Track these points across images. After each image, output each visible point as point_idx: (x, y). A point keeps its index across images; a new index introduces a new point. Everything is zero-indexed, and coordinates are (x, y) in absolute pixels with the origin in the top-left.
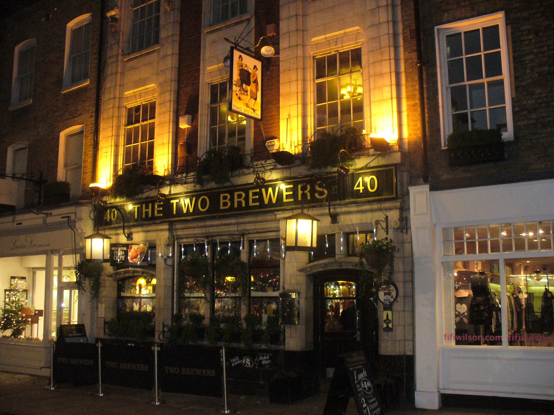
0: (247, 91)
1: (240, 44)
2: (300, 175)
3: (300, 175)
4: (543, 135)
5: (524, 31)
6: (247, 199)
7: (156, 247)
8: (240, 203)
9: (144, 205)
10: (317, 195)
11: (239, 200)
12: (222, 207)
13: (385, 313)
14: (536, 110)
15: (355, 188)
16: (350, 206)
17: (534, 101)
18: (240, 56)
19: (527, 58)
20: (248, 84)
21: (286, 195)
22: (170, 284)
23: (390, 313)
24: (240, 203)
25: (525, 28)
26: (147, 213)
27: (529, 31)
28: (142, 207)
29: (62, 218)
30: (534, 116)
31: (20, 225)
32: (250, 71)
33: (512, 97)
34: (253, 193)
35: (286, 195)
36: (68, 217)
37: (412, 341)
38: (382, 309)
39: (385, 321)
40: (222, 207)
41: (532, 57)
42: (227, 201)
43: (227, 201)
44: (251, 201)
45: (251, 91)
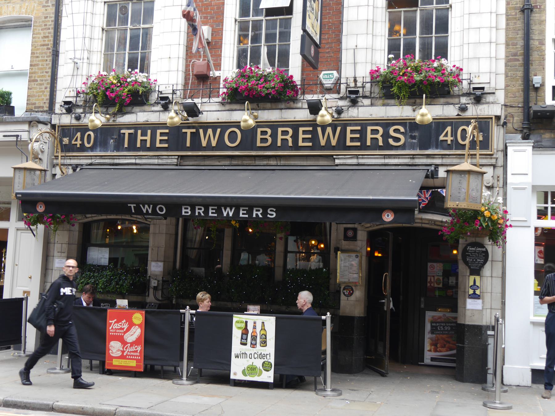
2: (370, 116)
3: (370, 116)
6: (295, 137)
7: (11, 204)
8: (284, 141)
12: (259, 144)
13: (472, 278)
16: (434, 157)
22: (173, 232)
23: (478, 278)
24: (284, 141)
28: (136, 133)
29: (4, 136)
33: (535, 263)
36: (17, 136)
38: (468, 274)
39: (471, 286)
40: (259, 144)
43: (267, 137)
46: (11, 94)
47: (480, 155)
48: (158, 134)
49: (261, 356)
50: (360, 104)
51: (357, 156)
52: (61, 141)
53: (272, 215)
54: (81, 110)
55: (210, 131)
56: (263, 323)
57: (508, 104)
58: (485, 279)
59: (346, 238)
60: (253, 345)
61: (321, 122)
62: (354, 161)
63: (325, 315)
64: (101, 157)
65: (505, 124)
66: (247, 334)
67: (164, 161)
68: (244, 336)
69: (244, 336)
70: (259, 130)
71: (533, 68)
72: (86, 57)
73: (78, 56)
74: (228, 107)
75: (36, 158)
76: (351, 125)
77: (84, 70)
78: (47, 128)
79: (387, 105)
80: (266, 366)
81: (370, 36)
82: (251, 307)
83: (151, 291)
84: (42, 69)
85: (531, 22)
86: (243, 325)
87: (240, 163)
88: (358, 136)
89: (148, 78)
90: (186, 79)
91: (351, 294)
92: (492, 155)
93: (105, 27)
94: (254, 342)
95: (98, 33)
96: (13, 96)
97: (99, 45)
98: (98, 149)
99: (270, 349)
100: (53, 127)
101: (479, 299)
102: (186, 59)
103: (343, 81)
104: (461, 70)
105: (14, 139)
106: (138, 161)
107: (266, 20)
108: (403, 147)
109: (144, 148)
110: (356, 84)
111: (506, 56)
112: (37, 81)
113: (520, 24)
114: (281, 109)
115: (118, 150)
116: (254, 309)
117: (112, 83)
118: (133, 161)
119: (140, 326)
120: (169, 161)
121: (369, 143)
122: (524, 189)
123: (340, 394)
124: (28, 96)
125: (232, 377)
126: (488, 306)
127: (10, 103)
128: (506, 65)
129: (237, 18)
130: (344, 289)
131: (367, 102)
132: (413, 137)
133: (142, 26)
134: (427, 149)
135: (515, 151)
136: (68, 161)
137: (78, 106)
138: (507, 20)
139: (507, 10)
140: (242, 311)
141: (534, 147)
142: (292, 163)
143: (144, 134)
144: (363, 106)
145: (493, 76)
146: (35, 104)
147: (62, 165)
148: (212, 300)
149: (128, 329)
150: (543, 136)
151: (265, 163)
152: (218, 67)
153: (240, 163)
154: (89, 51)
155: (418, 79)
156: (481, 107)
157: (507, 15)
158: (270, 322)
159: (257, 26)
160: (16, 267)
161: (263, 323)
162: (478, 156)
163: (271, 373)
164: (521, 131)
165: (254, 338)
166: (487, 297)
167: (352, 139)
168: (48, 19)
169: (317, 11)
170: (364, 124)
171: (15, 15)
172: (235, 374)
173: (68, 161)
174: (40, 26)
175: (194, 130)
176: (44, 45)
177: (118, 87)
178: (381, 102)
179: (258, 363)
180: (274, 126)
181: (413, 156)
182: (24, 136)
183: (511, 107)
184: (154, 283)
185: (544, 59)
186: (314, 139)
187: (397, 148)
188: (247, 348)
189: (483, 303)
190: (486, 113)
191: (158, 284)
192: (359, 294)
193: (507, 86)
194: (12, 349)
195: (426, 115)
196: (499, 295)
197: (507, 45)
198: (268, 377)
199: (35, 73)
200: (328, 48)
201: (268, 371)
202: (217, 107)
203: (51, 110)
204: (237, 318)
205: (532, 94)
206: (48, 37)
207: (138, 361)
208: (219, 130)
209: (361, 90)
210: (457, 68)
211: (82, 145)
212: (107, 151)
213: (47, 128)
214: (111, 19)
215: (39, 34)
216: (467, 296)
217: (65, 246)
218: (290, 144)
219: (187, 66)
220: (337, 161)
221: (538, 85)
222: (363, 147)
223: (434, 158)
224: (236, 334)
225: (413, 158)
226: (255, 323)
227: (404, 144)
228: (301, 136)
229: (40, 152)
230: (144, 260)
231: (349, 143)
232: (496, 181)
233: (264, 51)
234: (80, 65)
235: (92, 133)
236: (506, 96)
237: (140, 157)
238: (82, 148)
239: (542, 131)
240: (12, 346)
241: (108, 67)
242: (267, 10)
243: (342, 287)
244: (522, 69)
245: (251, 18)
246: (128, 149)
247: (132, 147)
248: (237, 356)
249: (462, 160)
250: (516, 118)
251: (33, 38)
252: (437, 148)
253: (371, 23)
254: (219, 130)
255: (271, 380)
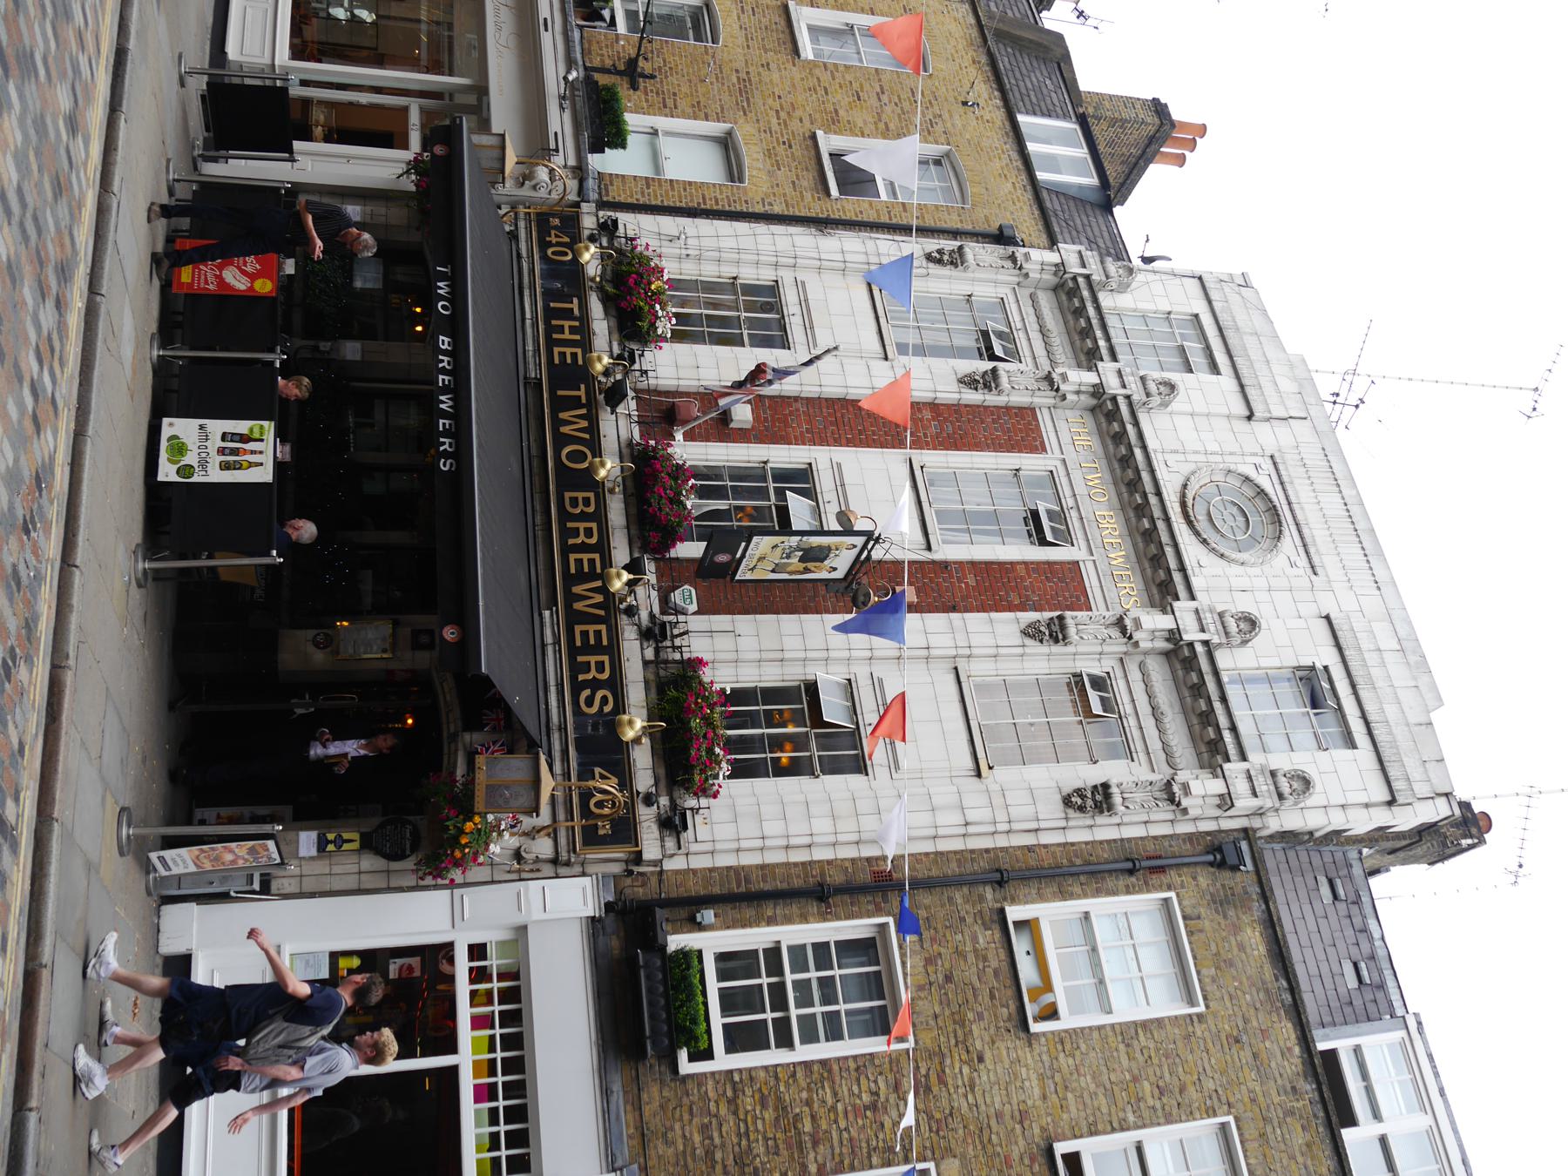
0: (788, 557)
1: (877, 546)
4: (687, 1128)
5: (876, 1082)
6: (584, 548)
8: (576, 532)
9: (577, 324)
10: (587, 692)
11: (580, 501)
12: (568, 495)
13: (356, 836)
14: (735, 1113)
15: (597, 770)
17: (749, 1108)
18: (855, 546)
19: (828, 1090)
20: (802, 560)
21: (565, 353)
23: (356, 845)
24: (576, 532)
25: (882, 1084)
26: (561, 329)
27: (877, 1094)
29: (545, 19)
30: (723, 1111)
31: (542, 28)
32: (826, 562)
34: (600, 632)
35: (565, 353)
36: (557, 150)
37: (298, 891)
38: (363, 830)
40: (568, 495)
41: (830, 1100)
42: (581, 507)
43: (581, 507)
44: (579, 556)
45: (790, 564)
46: (624, 147)
47: (573, 828)
48: (574, 350)
49: (203, 464)
50: (645, 645)
51: (557, 642)
52: (554, 216)
53: (445, 465)
54: (605, 243)
55: (584, 424)
56: (261, 464)
57: (665, 877)
58: (354, 858)
59: (416, 633)
60: (221, 451)
61: (608, 574)
62: (549, 639)
63: (279, 555)
64: (532, 271)
65: (630, 873)
66: (240, 442)
67: (531, 360)
68: (238, 438)
69: (238, 438)
70: (591, 495)
71: (730, 912)
72: (689, 252)
73: (690, 241)
74: (625, 451)
75: (525, 178)
76: (609, 630)
77: (667, 250)
78: (573, 197)
79: (647, 689)
80: (186, 470)
81: (757, 656)
82: (288, 448)
83: (312, 343)
84: (667, 195)
85: (803, 901)
86: (256, 435)
87: (535, 470)
88: (592, 642)
89: (664, 339)
90: (667, 393)
91: (317, 645)
92: (575, 851)
93: (739, 281)
94: (227, 451)
95: (728, 271)
96: (621, 151)
97: (709, 272)
98: (544, 267)
99: (216, 476)
100: (577, 205)
101: (319, 851)
102: (699, 393)
103: (681, 618)
104: (715, 796)
105: (552, 146)
106: (528, 322)
107: (770, 507)
108: (577, 711)
109: (550, 330)
110: (677, 636)
111: (743, 867)
112: (648, 188)
113: (797, 883)
114: (628, 527)
115: (543, 294)
116: (285, 453)
117: (650, 283)
118: (528, 315)
119: (251, 288)
120: (531, 366)
121: (580, 659)
122: (520, 909)
123: (139, 586)
124: (623, 176)
125: (166, 421)
126: (307, 869)
127: (610, 147)
128: (729, 868)
129: (770, 465)
130: (326, 635)
131: (650, 654)
132: (595, 727)
133: (745, 332)
134: (578, 749)
135: (584, 889)
136: (522, 224)
137: (611, 241)
138: (803, 864)
139: (819, 862)
140: (281, 434)
141: (593, 918)
142: (540, 548)
143: (573, 330)
144: (642, 649)
145: (708, 847)
146: (612, 184)
147: (516, 214)
148: (298, 400)
149: (244, 273)
150: (614, 937)
151: (538, 507)
152: (689, 437)
153: (535, 470)
154: (699, 258)
155: (693, 724)
156: (655, 827)
157: (811, 863)
158: (264, 475)
159: (762, 493)
160: (345, 160)
161: (261, 464)
162: (570, 824)
163: (174, 478)
164: (618, 899)
165: (235, 452)
166: (321, 867)
167: (585, 634)
168: (744, 205)
169: (789, 569)
170: (614, 650)
171: (747, 162)
172: (171, 425)
173: (522, 224)
174: (733, 194)
175: (584, 401)
176: (704, 198)
177: (646, 293)
178: (651, 677)
179: (191, 458)
180: (600, 516)
181: (563, 728)
182: (558, 161)
183: (660, 881)
184: (325, 346)
185: (744, 926)
186: (582, 577)
187: (576, 702)
188: (216, 442)
189: (312, 858)
190: (645, 836)
191: (324, 352)
192: (319, 657)
193: (694, 872)
194: (206, 134)
195: (632, 728)
196: (327, 888)
197: (763, 867)
198: (167, 472)
199: (660, 185)
200: (733, 597)
201: (178, 472)
202: (624, 434)
203: (602, 205)
204: (269, 427)
205: (683, 913)
206: (717, 203)
207: (191, 285)
208: (587, 436)
209: (668, 643)
210: (718, 792)
211: (550, 244)
212: (542, 277)
213: (573, 197)
214: (750, 289)
215: (721, 193)
216: (323, 831)
217: (383, 220)
218: (571, 541)
219: (688, 394)
220: (547, 613)
221: (699, 919)
222: (573, 651)
223: (563, 761)
224: (242, 427)
225: (560, 730)
226: (261, 452)
227: (584, 714)
228: (585, 557)
229: (533, 182)
230: (365, 334)
231: (578, 629)
232: (531, 867)
233: (721, 505)
234: (677, 243)
235: (569, 257)
236: (677, 872)
237: (535, 325)
238: (544, 245)
239: (622, 934)
240: (211, 134)
241: (674, 284)
242: (786, 508)
243: (329, 632)
244: (725, 891)
245: (772, 485)
246: (546, 308)
247: (550, 314)
248: (201, 427)
249: (559, 778)
250: (641, 890)
251: (714, 185)
252: (580, 765)
253: (779, 655)
254: (587, 436)
255: (161, 478)
